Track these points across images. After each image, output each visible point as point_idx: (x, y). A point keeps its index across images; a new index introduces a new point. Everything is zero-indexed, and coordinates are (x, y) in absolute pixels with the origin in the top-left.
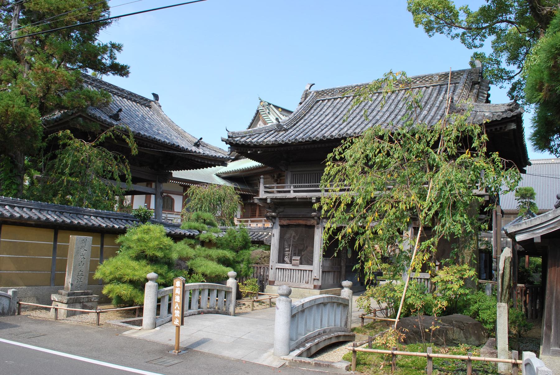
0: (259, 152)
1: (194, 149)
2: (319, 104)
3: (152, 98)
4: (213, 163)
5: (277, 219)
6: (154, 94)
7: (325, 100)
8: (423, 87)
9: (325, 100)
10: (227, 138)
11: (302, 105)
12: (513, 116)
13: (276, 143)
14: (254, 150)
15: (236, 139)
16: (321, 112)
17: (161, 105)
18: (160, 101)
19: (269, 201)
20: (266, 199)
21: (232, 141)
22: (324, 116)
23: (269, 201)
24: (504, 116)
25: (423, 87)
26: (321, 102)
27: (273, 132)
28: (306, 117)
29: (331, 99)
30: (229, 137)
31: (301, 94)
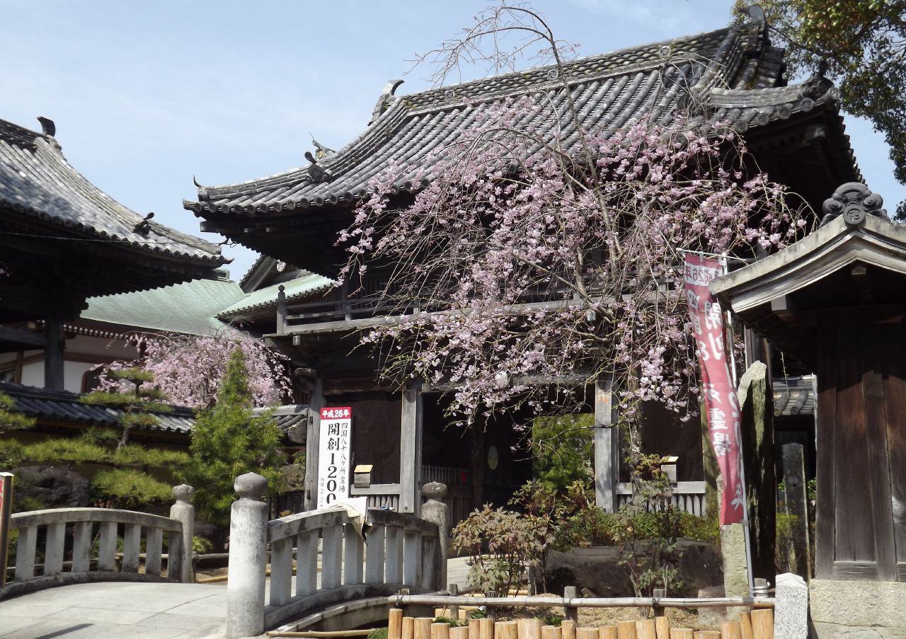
0: (268, 230)
1: (133, 238)
2: (411, 123)
3: (38, 128)
4: (182, 271)
5: (319, 382)
6: (42, 120)
7: (425, 115)
8: (638, 72)
9: (425, 115)
10: (196, 200)
11: (372, 126)
12: (816, 109)
13: (305, 206)
14: (258, 225)
15: (216, 203)
16: (415, 140)
17: (60, 144)
18: (58, 137)
19: (296, 341)
20: (291, 336)
21: (207, 208)
22: (418, 146)
23: (296, 341)
24: (798, 109)
25: (638, 72)
26: (416, 119)
27: (302, 184)
28: (380, 152)
29: (437, 112)
30: (201, 198)
31: (374, 103)
